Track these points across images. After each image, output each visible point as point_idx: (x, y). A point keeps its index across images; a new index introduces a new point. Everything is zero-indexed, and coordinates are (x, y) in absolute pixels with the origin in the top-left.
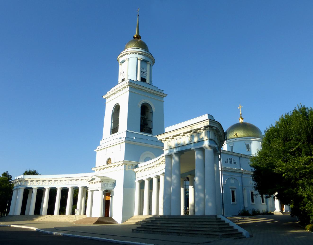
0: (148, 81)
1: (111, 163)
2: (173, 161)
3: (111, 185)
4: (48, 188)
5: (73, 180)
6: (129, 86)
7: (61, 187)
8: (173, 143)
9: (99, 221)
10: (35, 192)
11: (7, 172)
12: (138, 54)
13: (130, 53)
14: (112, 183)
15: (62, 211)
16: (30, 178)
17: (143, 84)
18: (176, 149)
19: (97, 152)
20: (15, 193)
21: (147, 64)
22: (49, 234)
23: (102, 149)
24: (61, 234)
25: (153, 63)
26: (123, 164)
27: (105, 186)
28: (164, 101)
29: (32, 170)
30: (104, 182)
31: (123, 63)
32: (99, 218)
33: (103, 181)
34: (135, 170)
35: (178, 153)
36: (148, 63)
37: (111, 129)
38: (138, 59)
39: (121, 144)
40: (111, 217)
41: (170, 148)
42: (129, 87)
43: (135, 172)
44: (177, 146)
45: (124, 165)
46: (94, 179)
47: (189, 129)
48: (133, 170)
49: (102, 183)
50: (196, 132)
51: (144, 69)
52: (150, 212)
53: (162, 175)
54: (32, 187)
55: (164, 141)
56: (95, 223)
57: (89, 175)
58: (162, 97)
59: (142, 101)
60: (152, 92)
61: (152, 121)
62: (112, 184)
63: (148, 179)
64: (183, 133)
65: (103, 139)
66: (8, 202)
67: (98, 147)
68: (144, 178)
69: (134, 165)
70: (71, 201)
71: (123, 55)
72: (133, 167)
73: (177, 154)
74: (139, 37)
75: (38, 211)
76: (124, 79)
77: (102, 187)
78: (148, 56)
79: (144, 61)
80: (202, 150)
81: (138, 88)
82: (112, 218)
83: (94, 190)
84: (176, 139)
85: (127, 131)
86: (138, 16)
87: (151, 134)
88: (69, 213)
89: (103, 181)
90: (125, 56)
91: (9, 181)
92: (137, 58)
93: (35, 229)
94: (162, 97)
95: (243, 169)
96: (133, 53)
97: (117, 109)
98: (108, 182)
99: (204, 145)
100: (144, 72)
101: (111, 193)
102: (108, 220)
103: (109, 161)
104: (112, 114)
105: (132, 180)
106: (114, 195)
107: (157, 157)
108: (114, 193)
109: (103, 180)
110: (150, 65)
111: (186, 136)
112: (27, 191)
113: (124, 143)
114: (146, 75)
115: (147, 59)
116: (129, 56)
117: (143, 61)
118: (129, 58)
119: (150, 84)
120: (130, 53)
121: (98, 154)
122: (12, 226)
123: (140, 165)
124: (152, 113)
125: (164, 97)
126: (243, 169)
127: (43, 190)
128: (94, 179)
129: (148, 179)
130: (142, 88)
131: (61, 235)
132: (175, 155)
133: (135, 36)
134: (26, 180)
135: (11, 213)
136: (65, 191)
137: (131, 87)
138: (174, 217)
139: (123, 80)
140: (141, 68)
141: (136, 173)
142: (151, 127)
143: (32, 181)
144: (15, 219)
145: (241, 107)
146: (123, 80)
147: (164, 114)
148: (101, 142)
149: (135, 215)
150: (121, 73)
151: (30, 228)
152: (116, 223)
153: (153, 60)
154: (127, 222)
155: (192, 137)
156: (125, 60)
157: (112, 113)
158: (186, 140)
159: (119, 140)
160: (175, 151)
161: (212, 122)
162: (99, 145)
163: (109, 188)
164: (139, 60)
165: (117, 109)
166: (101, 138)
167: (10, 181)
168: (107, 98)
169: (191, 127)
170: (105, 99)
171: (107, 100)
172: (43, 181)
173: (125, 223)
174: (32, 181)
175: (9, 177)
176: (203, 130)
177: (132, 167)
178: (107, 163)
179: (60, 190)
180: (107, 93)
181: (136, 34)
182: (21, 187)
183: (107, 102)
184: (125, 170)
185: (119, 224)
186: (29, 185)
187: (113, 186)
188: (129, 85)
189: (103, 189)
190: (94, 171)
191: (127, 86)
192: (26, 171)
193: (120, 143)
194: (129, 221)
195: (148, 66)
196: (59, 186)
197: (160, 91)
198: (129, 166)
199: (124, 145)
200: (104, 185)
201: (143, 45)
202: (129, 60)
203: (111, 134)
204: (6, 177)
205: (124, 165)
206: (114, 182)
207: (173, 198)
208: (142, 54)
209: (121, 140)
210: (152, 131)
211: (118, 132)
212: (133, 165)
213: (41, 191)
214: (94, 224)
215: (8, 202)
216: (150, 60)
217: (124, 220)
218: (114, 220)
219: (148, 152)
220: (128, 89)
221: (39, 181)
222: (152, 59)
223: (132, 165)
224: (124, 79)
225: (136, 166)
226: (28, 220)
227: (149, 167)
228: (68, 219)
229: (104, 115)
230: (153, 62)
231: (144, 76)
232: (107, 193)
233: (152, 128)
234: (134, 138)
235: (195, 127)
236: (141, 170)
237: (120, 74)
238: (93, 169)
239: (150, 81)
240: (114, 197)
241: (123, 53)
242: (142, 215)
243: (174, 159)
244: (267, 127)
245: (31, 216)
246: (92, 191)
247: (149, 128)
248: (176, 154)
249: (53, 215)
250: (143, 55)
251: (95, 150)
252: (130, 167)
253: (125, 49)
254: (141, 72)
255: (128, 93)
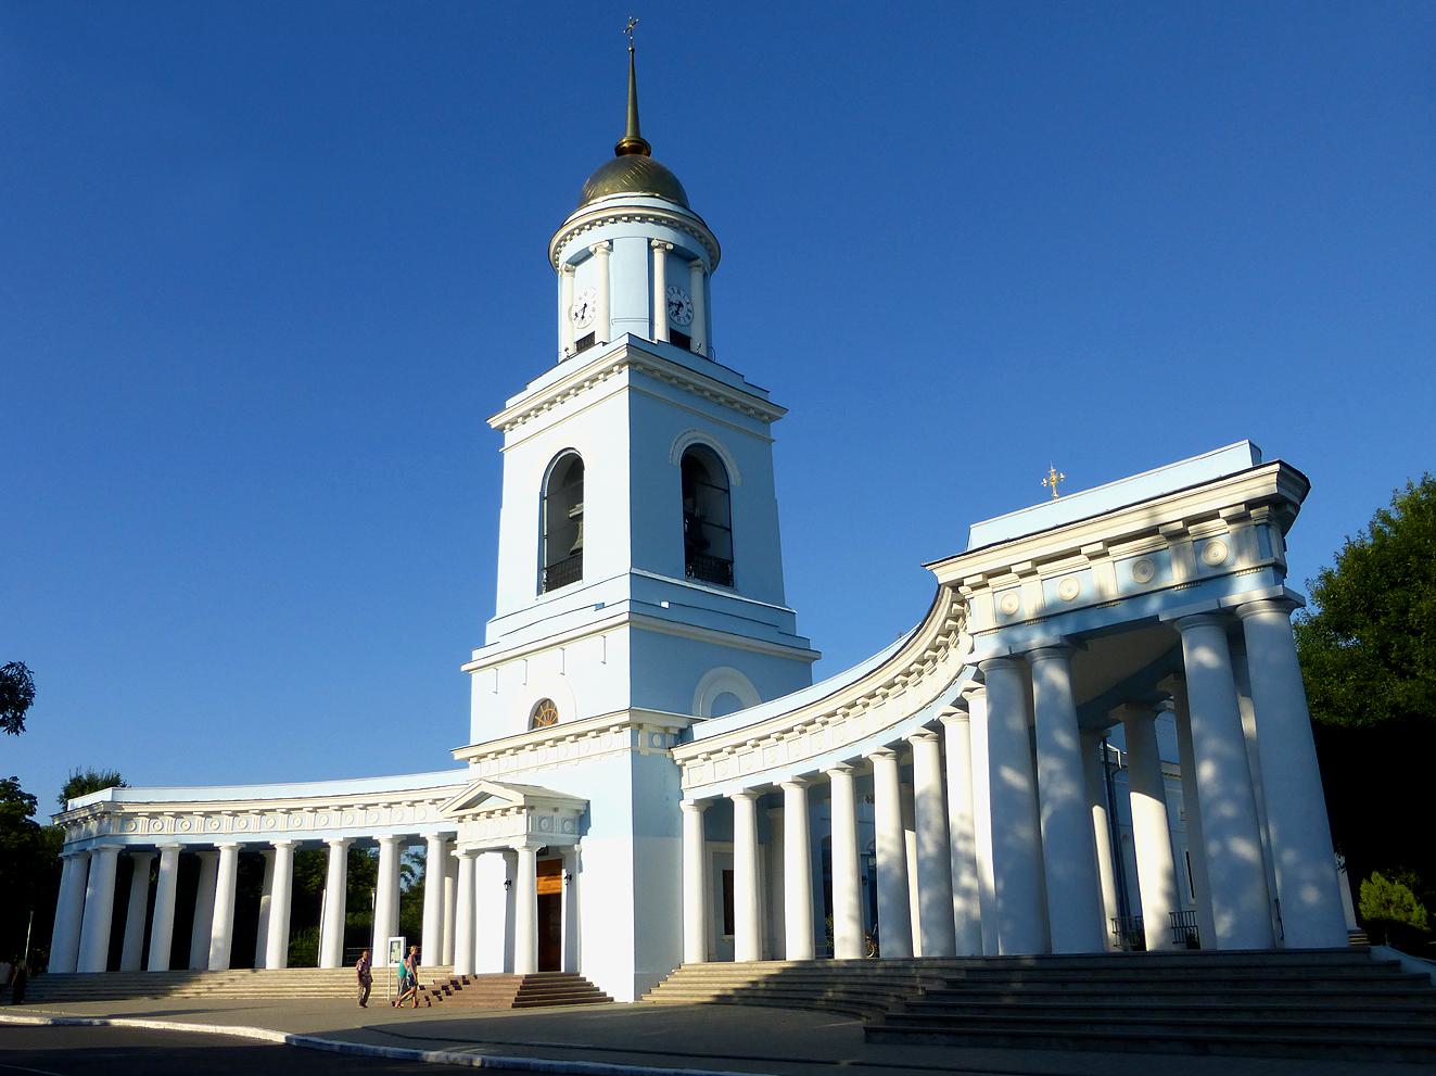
0: (697, 342)
1: (556, 721)
2: (1036, 688)
3: (568, 826)
4: (231, 848)
5: (400, 803)
6: (629, 363)
7: (346, 839)
8: (1028, 598)
9: (530, 992)
10: (168, 865)
11: (15, 779)
12: (639, 221)
13: (617, 219)
14: (572, 815)
15: (302, 952)
16: (148, 803)
17: (677, 354)
18: (1046, 631)
19: (475, 676)
20: (71, 871)
21: (690, 267)
22: (398, 1060)
23: (506, 657)
24: (483, 1061)
25: (711, 258)
26: (624, 725)
27: (541, 830)
28: (773, 436)
29: (101, 771)
30: (539, 812)
31: (577, 264)
32: (527, 976)
33: (532, 808)
34: (680, 753)
35: (1065, 643)
36: (694, 263)
37: (540, 569)
38: (654, 243)
39: (608, 634)
40: (573, 975)
41: (1009, 623)
42: (626, 369)
43: (679, 762)
44: (1047, 617)
45: (627, 731)
46: (483, 797)
47: (1138, 522)
48: (669, 756)
49: (528, 816)
50: (1181, 537)
51: (679, 293)
52: (771, 944)
53: (843, 770)
54: (158, 842)
55: (974, 588)
56: (516, 1000)
57: (454, 784)
58: (764, 422)
59: (685, 438)
60: (727, 394)
61: (730, 530)
62: (573, 821)
63: (750, 791)
64: (1030, 563)
65: (499, 614)
66: (32, 913)
67: (476, 654)
68: (733, 790)
69: (671, 731)
70: (395, 900)
71: (581, 228)
72: (670, 740)
73: (1059, 651)
74: (640, 147)
75: (184, 958)
76: (594, 333)
77: (529, 836)
78: (696, 234)
79: (678, 257)
80: (1231, 627)
81: (666, 377)
82: (581, 976)
83: (483, 851)
84: (1044, 577)
85: (634, 571)
86: (633, 50)
87: (728, 589)
88: (337, 961)
89: (532, 808)
90: (571, 239)
91: (25, 818)
92: (650, 241)
93: (279, 1038)
94: (764, 422)
95: (1116, 750)
96: (630, 218)
97: (567, 475)
98: (556, 810)
99: (1234, 599)
100: (680, 305)
101: (567, 862)
102: (567, 986)
103: (543, 714)
104: (542, 498)
105: (668, 799)
106: (581, 871)
107: (768, 695)
108: (581, 862)
109: (536, 803)
110: (705, 275)
111: (1115, 559)
112: (135, 862)
113: (626, 629)
114: (688, 321)
115: (694, 247)
116: (609, 230)
117: (676, 256)
118: (611, 242)
119: (707, 359)
120: (617, 219)
121: (481, 684)
122: (115, 1022)
123: (699, 730)
124: (728, 491)
125: (773, 418)
126: (1116, 750)
127: (198, 857)
128: (483, 797)
129: (750, 791)
130: (684, 376)
131: (482, 1066)
132: (1045, 654)
133: (625, 145)
134: (128, 809)
135: (58, 963)
136: (309, 859)
137: (639, 368)
138: (1077, 963)
139: (585, 343)
140: (668, 285)
141: (680, 768)
142: (725, 556)
143: (153, 816)
144: (77, 987)
145: (1059, 479)
146: (585, 343)
147: (776, 496)
148: (493, 631)
149: (686, 962)
150: (570, 309)
151: (242, 1034)
152: (602, 998)
153: (712, 254)
154: (657, 995)
155: (1150, 562)
156: (591, 249)
157: (542, 494)
158: (1111, 578)
159: (591, 615)
160: (1037, 638)
161: (1287, 476)
162: (481, 644)
163: (559, 838)
164: (656, 250)
165: (567, 475)
166: (488, 610)
167: (27, 820)
168: (507, 426)
169: (1145, 513)
170: (501, 429)
171: (510, 438)
172: (207, 815)
173: (649, 999)
174: (153, 816)
175: (26, 802)
176: (1230, 521)
177: (663, 736)
178: (534, 724)
179: (289, 852)
180: (509, 403)
181: (629, 133)
182: (104, 846)
183: (507, 445)
184: (635, 754)
185: (618, 1008)
186: (140, 833)
187: (577, 829)
188: (629, 359)
189: (532, 843)
190: (464, 764)
191: (621, 364)
192: (74, 776)
193: (559, 643)
194: (665, 989)
195: (697, 277)
196: (281, 836)
197: (756, 393)
198: (652, 735)
199: (621, 638)
200: (540, 827)
201: (660, 182)
202: (611, 250)
203: (539, 592)
204: (10, 799)
205: (627, 731)
206: (578, 811)
207: (1060, 869)
208: (670, 224)
209: (603, 613)
210: (732, 575)
211: (578, 576)
212: (666, 729)
213: (254, 862)
214: (514, 1006)
215: (32, 913)
216: (706, 255)
217: (643, 984)
218: (590, 984)
219: (730, 671)
220: (622, 379)
221: (189, 817)
222: (709, 247)
223: (662, 731)
224: (594, 333)
225: (684, 736)
226: (148, 995)
227: (734, 743)
228: (340, 986)
229: (500, 505)
230: (714, 260)
231: (682, 322)
232: (551, 863)
233: (730, 559)
234: (665, 605)
235: (1172, 514)
236: (736, 746)
237: (570, 315)
238: (459, 755)
239: (708, 348)
240: (582, 879)
241: (579, 217)
242: (732, 959)
243: (1040, 678)
244: (1359, 532)
245: (157, 974)
246: (473, 854)
247: (718, 560)
248: (1051, 651)
249: (261, 971)
250: (674, 228)
251: (464, 668)
252: (657, 740)
253: (583, 201)
254: (669, 304)
255: (624, 398)
